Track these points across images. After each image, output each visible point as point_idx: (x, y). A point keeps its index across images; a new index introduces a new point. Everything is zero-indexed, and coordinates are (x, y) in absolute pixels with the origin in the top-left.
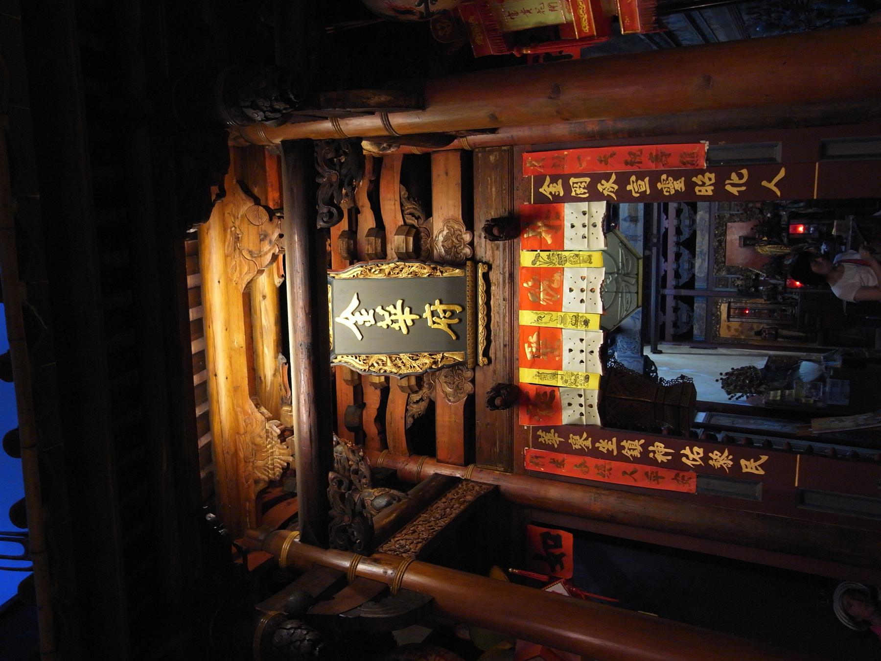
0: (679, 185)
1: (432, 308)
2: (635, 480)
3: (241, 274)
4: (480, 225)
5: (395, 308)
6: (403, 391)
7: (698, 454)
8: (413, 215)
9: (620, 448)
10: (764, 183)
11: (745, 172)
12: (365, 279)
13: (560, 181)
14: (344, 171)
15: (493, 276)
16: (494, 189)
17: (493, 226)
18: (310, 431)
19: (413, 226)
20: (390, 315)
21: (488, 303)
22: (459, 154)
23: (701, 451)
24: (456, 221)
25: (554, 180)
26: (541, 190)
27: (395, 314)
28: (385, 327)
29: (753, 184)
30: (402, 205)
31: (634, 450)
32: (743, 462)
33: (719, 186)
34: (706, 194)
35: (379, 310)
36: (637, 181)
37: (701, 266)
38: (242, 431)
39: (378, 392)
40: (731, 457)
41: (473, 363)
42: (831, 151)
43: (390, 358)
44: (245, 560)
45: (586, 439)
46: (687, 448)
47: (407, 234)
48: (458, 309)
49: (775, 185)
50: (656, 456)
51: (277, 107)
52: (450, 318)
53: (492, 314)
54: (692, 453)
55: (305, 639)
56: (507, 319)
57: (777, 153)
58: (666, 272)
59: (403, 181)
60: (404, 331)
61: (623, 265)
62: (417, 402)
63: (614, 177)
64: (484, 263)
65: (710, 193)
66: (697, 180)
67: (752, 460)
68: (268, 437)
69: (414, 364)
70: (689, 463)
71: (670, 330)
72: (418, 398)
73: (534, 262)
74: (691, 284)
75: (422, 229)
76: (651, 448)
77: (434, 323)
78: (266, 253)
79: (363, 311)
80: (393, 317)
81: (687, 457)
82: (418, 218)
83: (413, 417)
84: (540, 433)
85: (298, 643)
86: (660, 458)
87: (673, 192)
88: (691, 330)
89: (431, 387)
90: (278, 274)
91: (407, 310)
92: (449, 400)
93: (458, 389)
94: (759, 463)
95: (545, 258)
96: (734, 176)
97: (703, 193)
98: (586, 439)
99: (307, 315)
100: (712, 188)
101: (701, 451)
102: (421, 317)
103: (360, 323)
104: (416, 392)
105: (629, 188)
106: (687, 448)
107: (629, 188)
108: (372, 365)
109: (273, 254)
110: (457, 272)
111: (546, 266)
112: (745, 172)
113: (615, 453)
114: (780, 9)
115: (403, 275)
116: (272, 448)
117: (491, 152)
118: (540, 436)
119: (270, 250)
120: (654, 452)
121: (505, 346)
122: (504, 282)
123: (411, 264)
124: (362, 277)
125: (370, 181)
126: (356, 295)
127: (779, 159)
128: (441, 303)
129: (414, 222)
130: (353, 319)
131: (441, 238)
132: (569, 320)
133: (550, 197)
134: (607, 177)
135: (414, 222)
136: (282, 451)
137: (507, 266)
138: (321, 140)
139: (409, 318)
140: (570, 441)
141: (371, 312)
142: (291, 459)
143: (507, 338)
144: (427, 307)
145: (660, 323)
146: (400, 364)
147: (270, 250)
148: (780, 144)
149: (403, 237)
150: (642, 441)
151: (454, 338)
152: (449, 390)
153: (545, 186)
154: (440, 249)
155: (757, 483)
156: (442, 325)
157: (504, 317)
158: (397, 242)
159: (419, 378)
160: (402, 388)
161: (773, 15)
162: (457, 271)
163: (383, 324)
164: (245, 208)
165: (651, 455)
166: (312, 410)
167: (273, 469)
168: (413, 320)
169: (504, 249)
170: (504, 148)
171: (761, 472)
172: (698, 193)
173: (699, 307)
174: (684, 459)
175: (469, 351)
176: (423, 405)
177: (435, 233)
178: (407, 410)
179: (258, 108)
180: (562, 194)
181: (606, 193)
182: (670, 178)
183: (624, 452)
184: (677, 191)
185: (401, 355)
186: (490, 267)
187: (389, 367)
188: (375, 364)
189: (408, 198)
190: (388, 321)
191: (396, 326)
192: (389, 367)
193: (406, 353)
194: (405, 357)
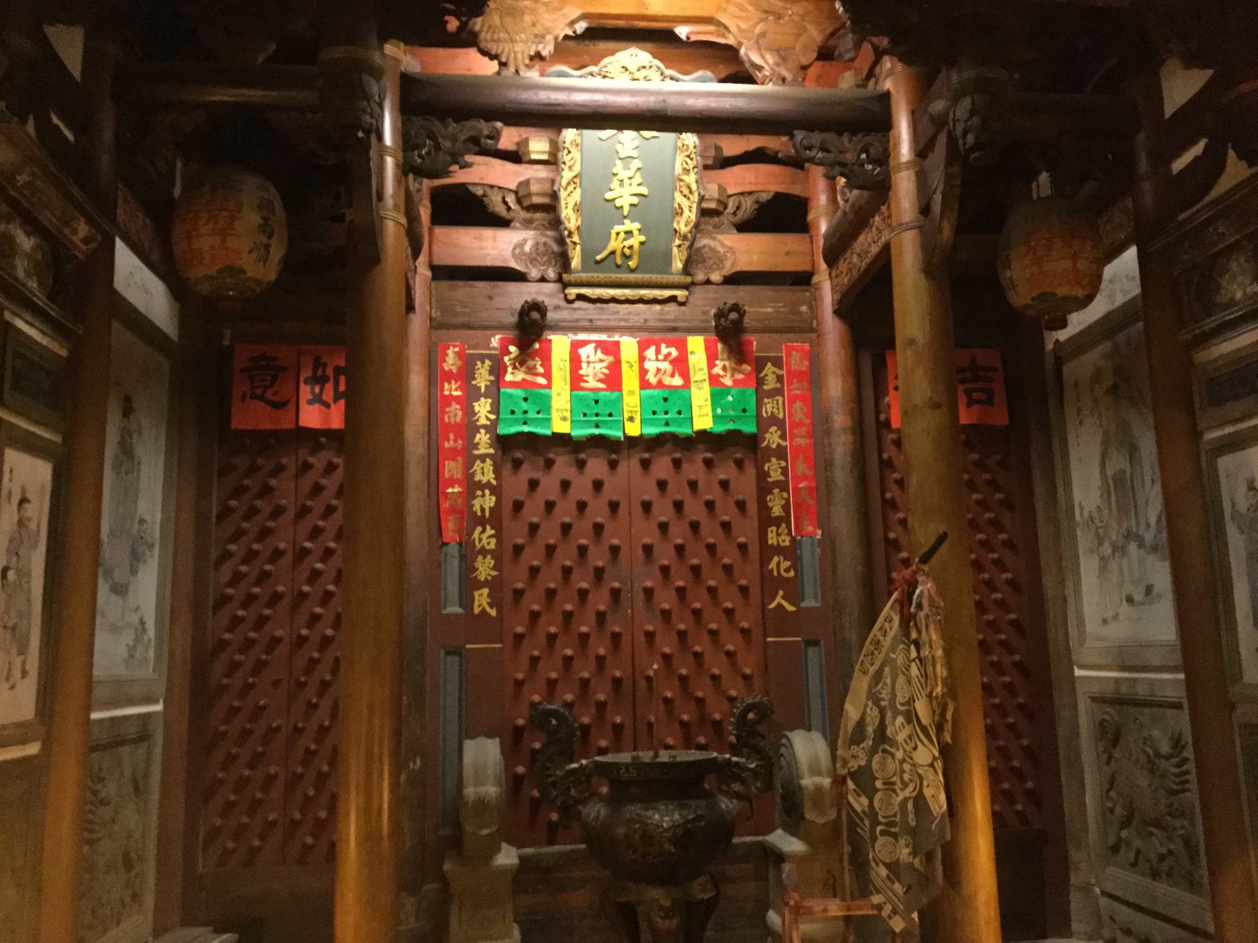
1: (636, 233)
4: (741, 294)
6: (520, 184)
9: (483, 458)
10: (781, 593)
14: (856, 168)
15: (672, 307)
16: (770, 310)
18: (559, 105)
19: (726, 208)
21: (641, 301)
23: (492, 546)
24: (733, 264)
25: (780, 379)
26: (769, 365)
28: (615, 171)
30: (750, 193)
32: (485, 591)
33: (779, 550)
35: (636, 164)
39: (512, 147)
42: (812, 651)
45: (488, 419)
46: (493, 532)
47: (719, 201)
48: (632, 264)
49: (780, 605)
52: (623, 254)
53: (627, 305)
56: (622, 324)
57: (809, 602)
59: (778, 196)
60: (609, 196)
62: (505, 203)
68: (536, 36)
69: (571, 206)
72: (511, 204)
75: (722, 218)
76: (487, 492)
77: (618, 234)
78: (763, 58)
80: (627, 182)
81: (484, 531)
82: (734, 214)
83: (485, 195)
84: (488, 362)
86: (477, 504)
87: (770, 504)
89: (528, 224)
90: (692, 33)
91: (635, 200)
94: (488, 609)
96: (788, 564)
97: (770, 535)
98: (488, 419)
99: (701, 112)
101: (492, 546)
102: (625, 217)
105: (774, 460)
106: (493, 532)
107: (774, 460)
110: (678, 265)
112: (792, 574)
115: (679, 198)
116: (522, 41)
117: (811, 307)
118: (483, 363)
119: (767, 62)
120: (483, 496)
121: (591, 321)
122: (666, 321)
125: (777, 153)
127: (803, 605)
128: (642, 243)
129: (730, 209)
131: (712, 244)
134: (783, 437)
135: (730, 209)
136: (519, 56)
139: (625, 201)
140: (482, 399)
141: (635, 154)
143: (599, 323)
147: (767, 62)
148: (818, 605)
149: (716, 195)
150: (494, 482)
151: (599, 258)
152: (527, 248)
154: (704, 242)
156: (614, 244)
157: (626, 320)
163: (618, 167)
164: (815, 33)
165: (479, 493)
166: (584, 110)
171: (477, 610)
174: (479, 529)
175: (584, 276)
176: (500, 210)
177: (719, 237)
178: (492, 187)
179: (972, 113)
180: (765, 387)
181: (767, 435)
183: (478, 462)
185: (578, 191)
186: (682, 304)
187: (567, 175)
188: (570, 156)
189: (757, 202)
190: (623, 175)
191: (615, 184)
194: (577, 196)
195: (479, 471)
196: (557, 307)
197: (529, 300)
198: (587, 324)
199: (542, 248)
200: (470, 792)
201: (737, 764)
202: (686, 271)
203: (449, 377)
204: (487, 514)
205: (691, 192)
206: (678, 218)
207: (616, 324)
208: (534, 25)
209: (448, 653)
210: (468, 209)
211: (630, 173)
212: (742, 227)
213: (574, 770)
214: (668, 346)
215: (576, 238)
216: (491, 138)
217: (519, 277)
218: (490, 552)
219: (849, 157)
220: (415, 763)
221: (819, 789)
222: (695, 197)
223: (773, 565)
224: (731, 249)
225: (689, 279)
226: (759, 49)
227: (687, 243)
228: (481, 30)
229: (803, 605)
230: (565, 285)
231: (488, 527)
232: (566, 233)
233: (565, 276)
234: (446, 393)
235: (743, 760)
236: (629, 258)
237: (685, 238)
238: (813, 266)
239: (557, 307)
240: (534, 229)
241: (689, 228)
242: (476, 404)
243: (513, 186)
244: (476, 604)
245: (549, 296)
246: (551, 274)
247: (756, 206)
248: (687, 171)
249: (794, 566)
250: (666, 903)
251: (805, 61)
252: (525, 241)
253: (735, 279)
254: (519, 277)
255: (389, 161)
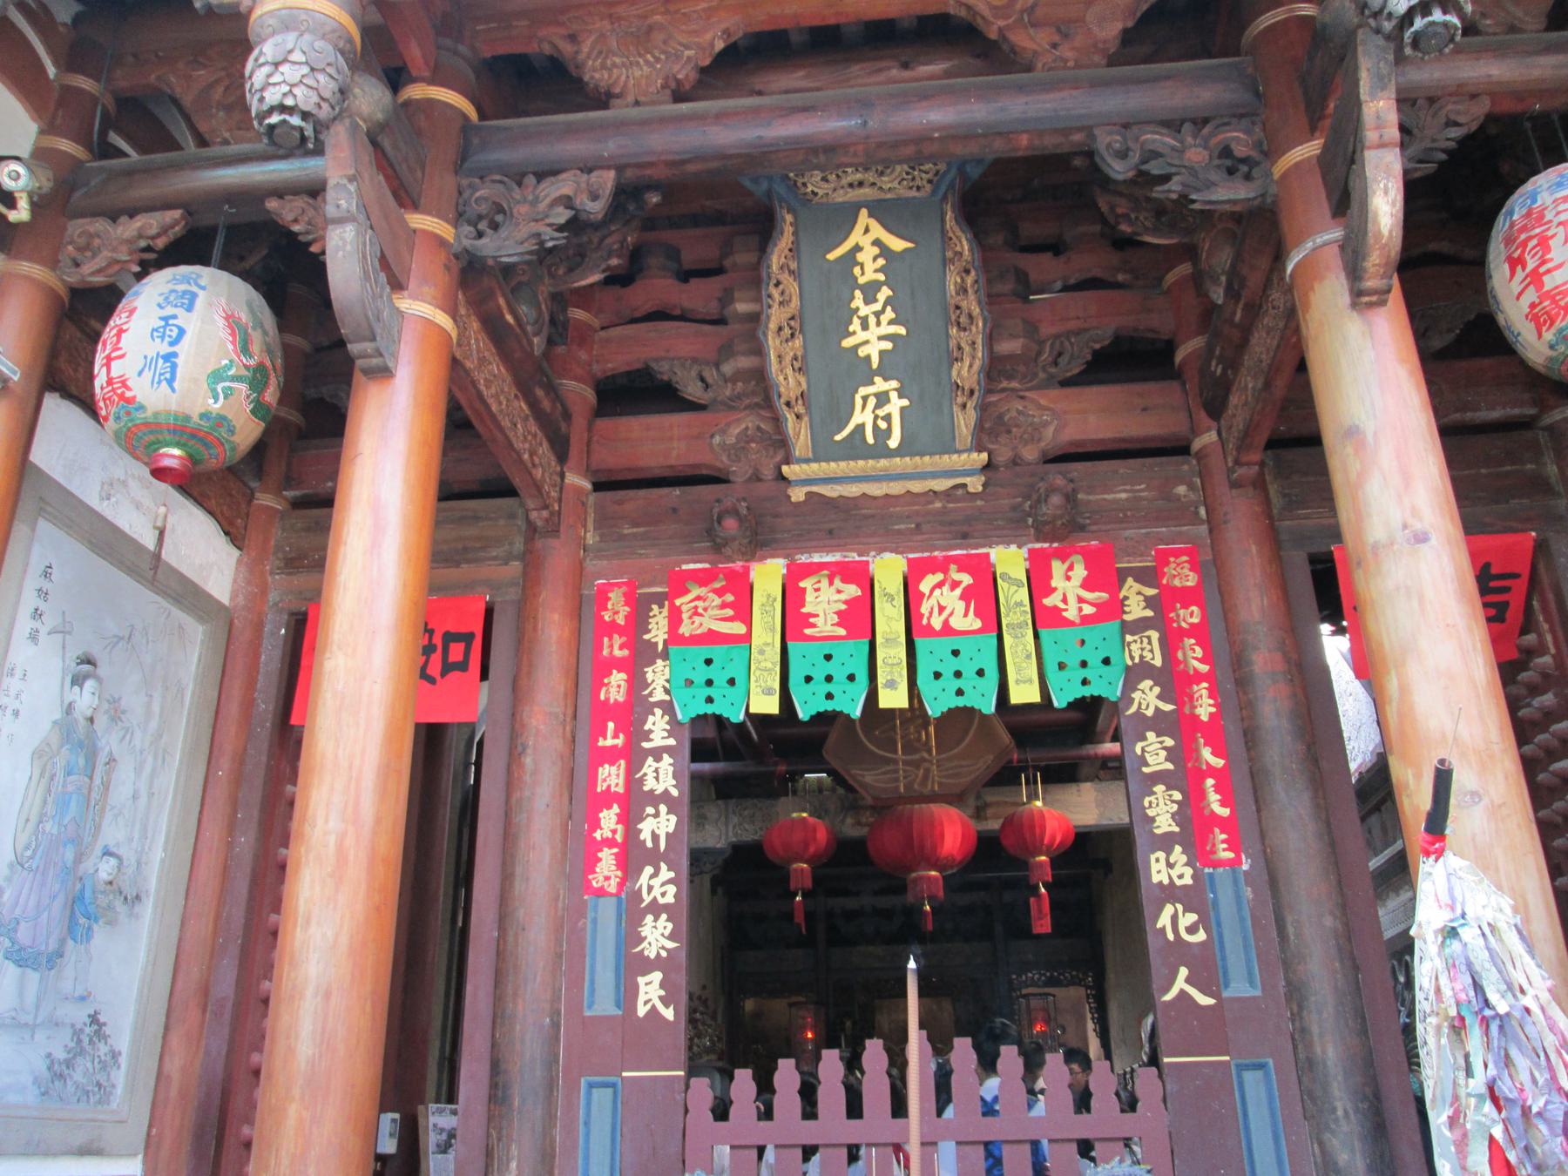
1: (894, 395)
7: (663, 894)
9: (657, 754)
10: (1183, 972)
11: (1201, 936)
16: (1124, 496)
20: (878, 314)
26: (1130, 581)
28: (853, 305)
31: (657, 779)
32: (657, 976)
35: (885, 292)
36: (1164, 748)
40: (664, 954)
46: (672, 874)
49: (1182, 992)
50: (650, 819)
54: (663, 885)
57: (1240, 987)
66: (1178, 853)
67: (662, 993)
70: (644, 880)
76: (663, 808)
77: (865, 399)
79: (881, 262)
80: (872, 320)
87: (1151, 813)
91: (888, 345)
96: (1192, 918)
97: (1154, 867)
103: (860, 257)
105: (1151, 735)
106: (672, 874)
112: (1201, 936)
113: (646, 745)
120: (657, 815)
124: (949, 254)
130: (865, 242)
139: (873, 350)
140: (660, 662)
142: (630, 99)
144: (894, 384)
148: (1258, 993)
150: (675, 792)
153: (1137, 587)
165: (650, 810)
167: (603, 67)
171: (642, 1011)
172: (1153, 857)
174: (649, 870)
181: (1136, 695)
182: (1175, 807)
183: (650, 760)
184: (1153, 820)
190: (865, 310)
191: (856, 325)
193: (805, 347)
203: (612, 628)
206: (956, 366)
211: (877, 307)
214: (960, 570)
218: (666, 908)
229: (1225, 994)
231: (664, 866)
233: (785, 469)
234: (605, 652)
242: (649, 670)
244: (641, 998)
249: (1203, 921)
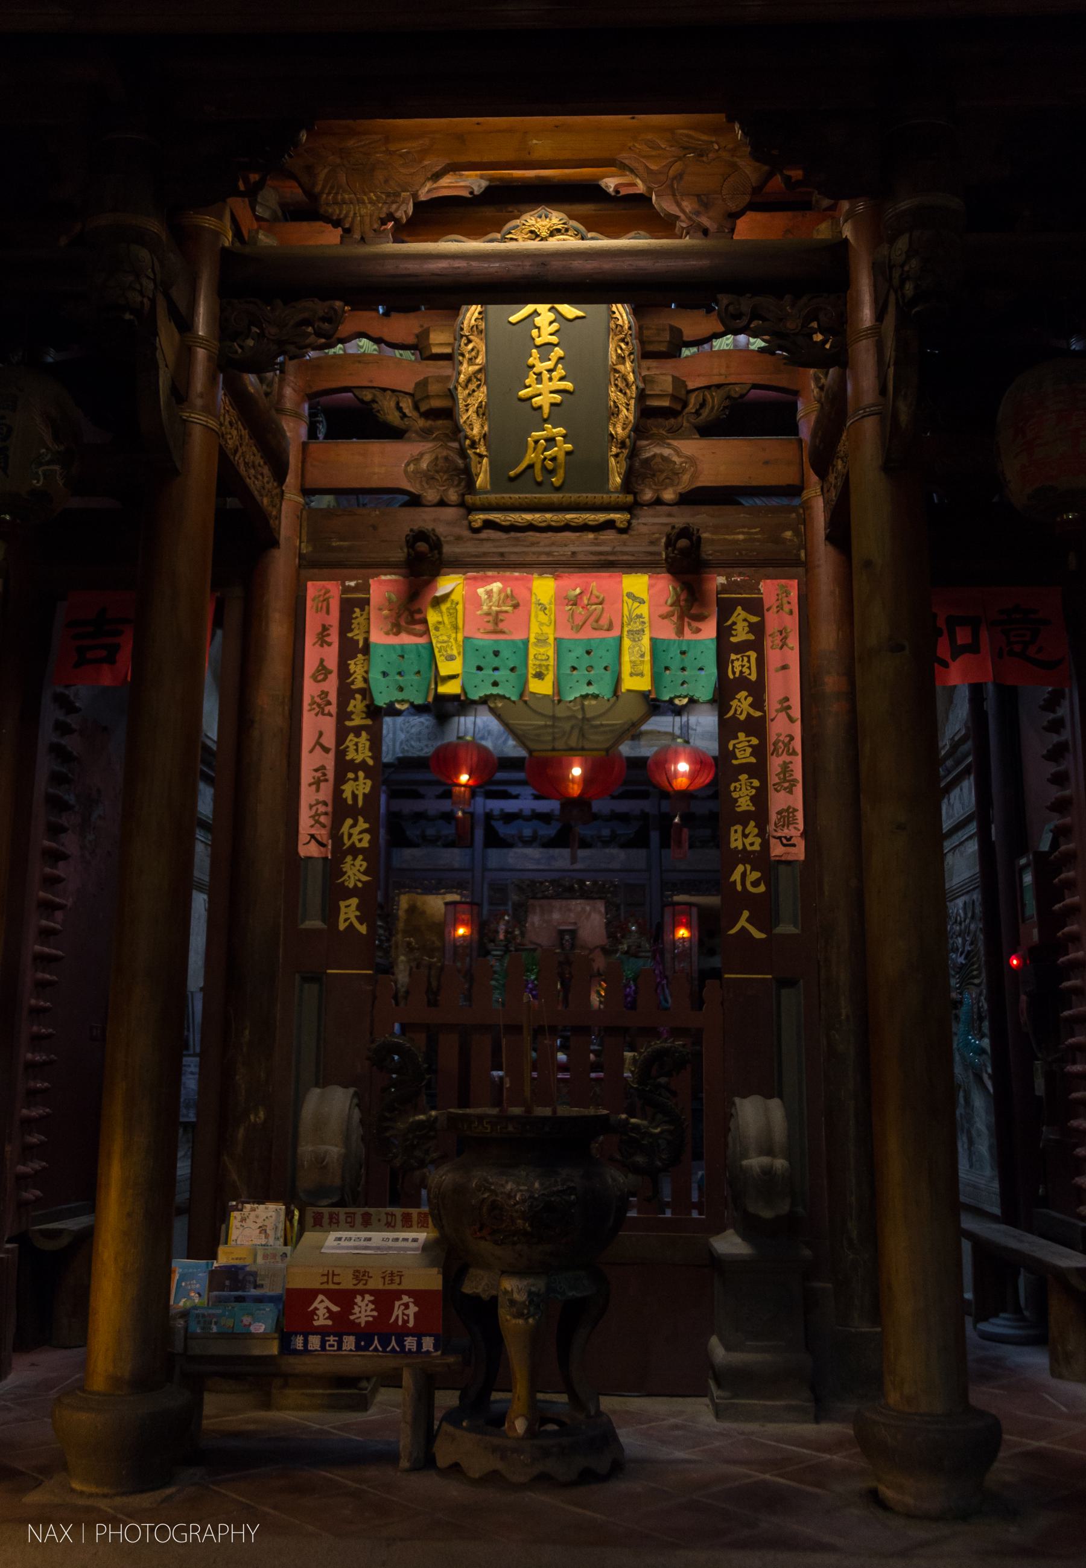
0: (744, 804)
2: (311, 751)
3: (644, 157)
4: (699, 518)
5: (562, 379)
6: (417, 384)
7: (360, 840)
8: (703, 405)
10: (746, 914)
11: (762, 888)
12: (609, 329)
13: (751, 637)
15: (609, 535)
17: (691, 540)
18: (409, 275)
19: (685, 404)
20: (550, 371)
22: (797, 482)
23: (365, 844)
24: (694, 477)
26: (739, 608)
27: (550, 379)
28: (531, 361)
29: (746, 899)
30: (719, 386)
31: (357, 750)
32: (354, 901)
34: (732, 839)
35: (558, 352)
36: (750, 746)
37: (527, 859)
38: (392, 147)
40: (360, 885)
41: (474, 504)
43: (480, 371)
44: (241, 194)
46: (367, 826)
47: (674, 398)
49: (743, 928)
50: (351, 782)
51: (907, 286)
52: (544, 467)
53: (550, 534)
54: (361, 833)
55: (143, 296)
56: (543, 558)
57: (786, 928)
58: (516, 797)
60: (523, 393)
61: (596, 727)
62: (399, 408)
63: (758, 714)
64: (629, 522)
65: (733, 845)
67: (358, 913)
68: (388, 195)
71: (408, 806)
72: (406, 411)
73: (630, 595)
74: (494, 840)
75: (680, 419)
76: (361, 774)
77: (536, 442)
78: (679, 205)
79: (555, 326)
80: (546, 375)
82: (697, 413)
83: (374, 401)
85: (138, 287)
86: (348, 789)
87: (735, 795)
88: (411, 844)
89: (425, 434)
91: (558, 398)
92: (408, 464)
93: (429, 477)
95: (638, 612)
96: (756, 875)
97: (733, 836)
100: (740, 847)
101: (365, 844)
102: (546, 421)
103: (538, 321)
104: (416, 407)
105: (741, 736)
106: (367, 826)
107: (741, 736)
108: (470, 341)
109: (677, 218)
111: (626, 612)
112: (762, 888)
113: (348, 723)
114: (968, 948)
115: (613, 394)
116: (371, 202)
117: (797, 533)
119: (683, 212)
120: (356, 779)
121: (502, 554)
122: (601, 553)
123: (632, 407)
126: (581, 314)
127: (780, 930)
129: (691, 407)
131: (666, 452)
132: (542, 650)
133: (729, 623)
135: (691, 407)
136: (367, 220)
137: (625, 558)
138: (846, 305)
139: (544, 401)
141: (554, 339)
143: (513, 558)
144: (561, 430)
145: (422, 790)
146: (472, 386)
147: (683, 212)
149: (670, 390)
150: (371, 762)
151: (512, 473)
152: (424, 465)
153: (744, 614)
154: (651, 450)
155: (324, 921)
156: (531, 456)
158: (664, 376)
159: (448, 414)
160: (423, 384)
161: (960, 940)
162: (618, 480)
164: (748, 171)
165: (351, 775)
167: (335, 203)
168: (540, 408)
169: (651, 553)
170: (803, 554)
171: (342, 926)
172: (733, 829)
173: (455, 857)
174: (349, 822)
175: (493, 498)
176: (394, 418)
177: (675, 443)
178: (384, 390)
180: (733, 639)
181: (734, 703)
182: (754, 791)
183: (351, 736)
184: (736, 800)
185: (484, 389)
186: (622, 531)
187: (467, 370)
188: (470, 346)
189: (729, 397)
190: (542, 367)
191: (531, 379)
192: (467, 370)
193: (488, 396)
194: (481, 395)
195: (352, 748)
196: (459, 538)
197: (415, 528)
198: (497, 559)
199: (441, 462)
200: (306, 1149)
201: (636, 1127)
202: (628, 486)
204: (360, 803)
205: (628, 385)
206: (614, 419)
207: (534, 558)
208: (386, 181)
209: (305, 980)
210: (353, 418)
211: (549, 364)
212: (706, 431)
213: (421, 1122)
215: (482, 449)
216: (329, 320)
217: (415, 501)
218: (362, 851)
219: (791, 325)
220: (256, 1115)
221: (768, 1172)
222: (633, 392)
223: (736, 876)
224: (692, 460)
225: (630, 498)
226: (674, 195)
227: (626, 452)
228: (322, 192)
229: (780, 930)
230: (471, 509)
232: (468, 442)
233: (469, 498)
235: (645, 1123)
236: (552, 472)
237: (623, 445)
238: (803, 481)
239: (459, 538)
240: (434, 440)
241: (627, 431)
242: (351, 662)
243: (410, 388)
245: (448, 523)
246: (453, 496)
247: (727, 403)
248: (621, 359)
250: (520, 1297)
251: (733, 207)
252: (421, 455)
253: (695, 498)
254: (415, 501)
255: (201, 353)
